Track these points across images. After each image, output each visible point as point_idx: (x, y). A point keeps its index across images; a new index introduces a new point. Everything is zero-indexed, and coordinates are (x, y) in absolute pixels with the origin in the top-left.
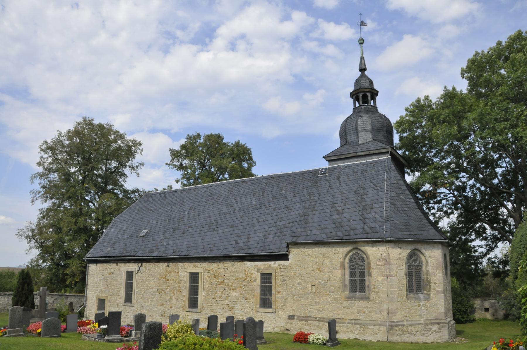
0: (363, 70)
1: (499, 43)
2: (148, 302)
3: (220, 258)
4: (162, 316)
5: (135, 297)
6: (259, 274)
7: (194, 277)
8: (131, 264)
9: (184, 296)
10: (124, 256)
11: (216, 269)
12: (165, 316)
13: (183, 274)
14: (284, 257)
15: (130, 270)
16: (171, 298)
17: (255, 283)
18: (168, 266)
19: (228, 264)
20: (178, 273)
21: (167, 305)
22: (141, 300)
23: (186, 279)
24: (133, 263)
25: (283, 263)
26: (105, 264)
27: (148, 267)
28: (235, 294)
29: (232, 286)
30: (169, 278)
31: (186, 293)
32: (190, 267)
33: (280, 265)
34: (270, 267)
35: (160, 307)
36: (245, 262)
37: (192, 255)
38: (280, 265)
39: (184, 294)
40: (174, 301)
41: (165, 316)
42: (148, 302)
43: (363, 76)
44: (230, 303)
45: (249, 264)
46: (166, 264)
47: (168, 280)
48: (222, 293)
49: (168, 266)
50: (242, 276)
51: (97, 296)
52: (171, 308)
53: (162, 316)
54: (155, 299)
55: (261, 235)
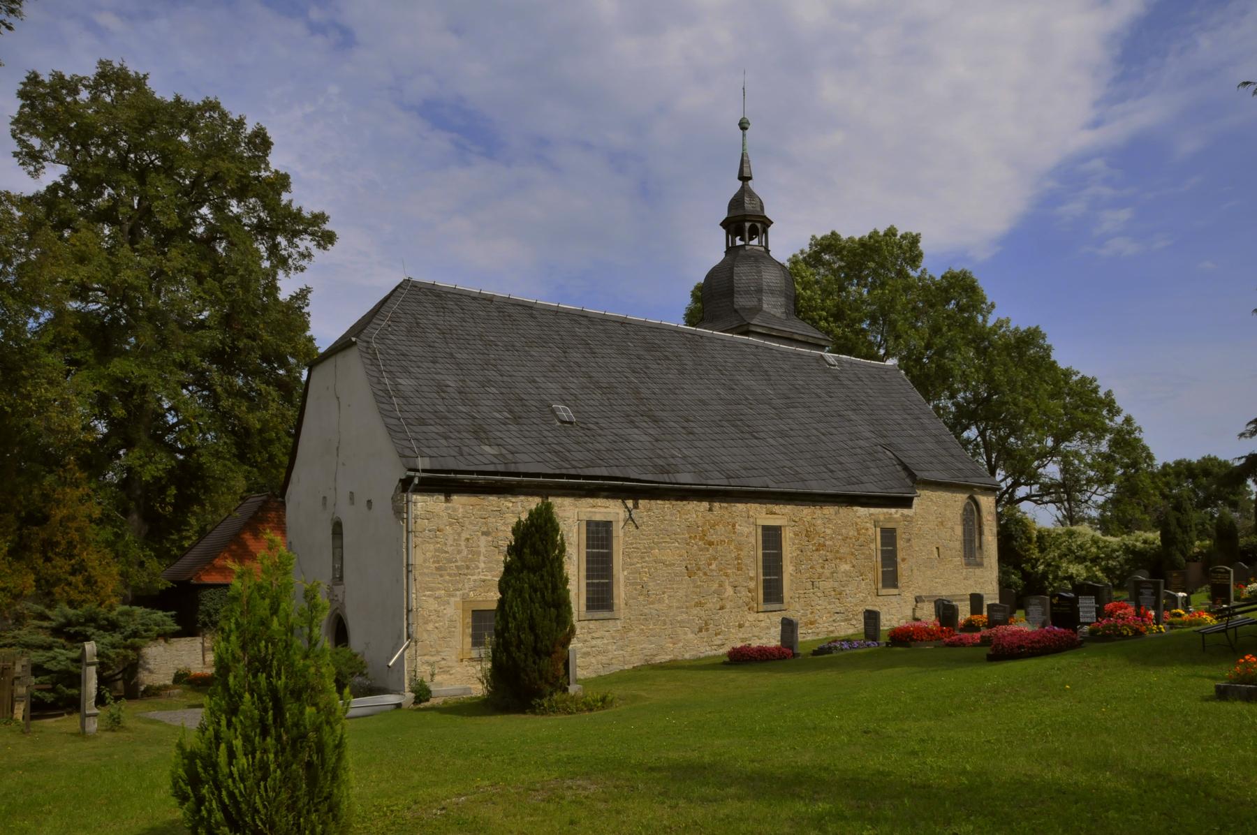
0: (744, 178)
1: (876, 232)
2: (660, 601)
3: (864, 500)
4: (700, 630)
5: (621, 592)
6: (878, 530)
7: (772, 536)
8: (600, 501)
9: (751, 579)
10: (503, 474)
11: (809, 518)
12: (707, 630)
13: (746, 530)
14: (906, 502)
15: (598, 518)
16: (720, 586)
17: (873, 546)
18: (710, 510)
19: (829, 510)
20: (734, 526)
21: (712, 603)
22: (641, 598)
23: (754, 540)
24: (607, 497)
25: (906, 511)
26: (493, 499)
27: (649, 510)
28: (845, 567)
29: (837, 552)
30: (714, 538)
31: (755, 570)
32: (763, 515)
33: (902, 515)
34: (890, 519)
35: (695, 611)
36: (855, 508)
37: (756, 483)
38: (902, 515)
39: (752, 574)
40: (729, 591)
41: (707, 630)
42: (660, 601)
43: (744, 192)
44: (836, 585)
45: (862, 511)
46: (706, 505)
47: (711, 544)
48: (823, 568)
49: (710, 510)
50: (852, 533)
51: (465, 600)
52: (722, 608)
53: (700, 630)
54: (681, 593)
55: (487, 448)
